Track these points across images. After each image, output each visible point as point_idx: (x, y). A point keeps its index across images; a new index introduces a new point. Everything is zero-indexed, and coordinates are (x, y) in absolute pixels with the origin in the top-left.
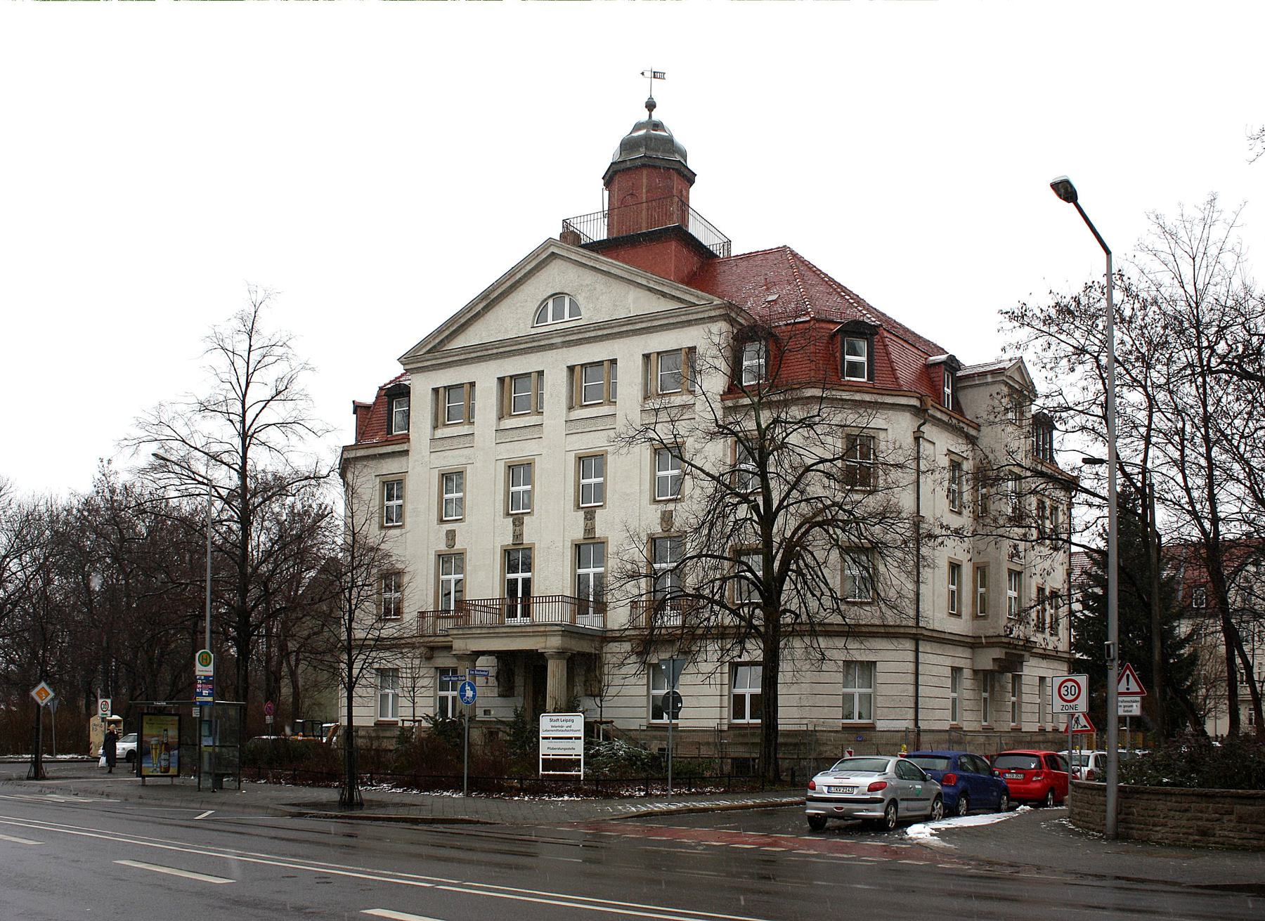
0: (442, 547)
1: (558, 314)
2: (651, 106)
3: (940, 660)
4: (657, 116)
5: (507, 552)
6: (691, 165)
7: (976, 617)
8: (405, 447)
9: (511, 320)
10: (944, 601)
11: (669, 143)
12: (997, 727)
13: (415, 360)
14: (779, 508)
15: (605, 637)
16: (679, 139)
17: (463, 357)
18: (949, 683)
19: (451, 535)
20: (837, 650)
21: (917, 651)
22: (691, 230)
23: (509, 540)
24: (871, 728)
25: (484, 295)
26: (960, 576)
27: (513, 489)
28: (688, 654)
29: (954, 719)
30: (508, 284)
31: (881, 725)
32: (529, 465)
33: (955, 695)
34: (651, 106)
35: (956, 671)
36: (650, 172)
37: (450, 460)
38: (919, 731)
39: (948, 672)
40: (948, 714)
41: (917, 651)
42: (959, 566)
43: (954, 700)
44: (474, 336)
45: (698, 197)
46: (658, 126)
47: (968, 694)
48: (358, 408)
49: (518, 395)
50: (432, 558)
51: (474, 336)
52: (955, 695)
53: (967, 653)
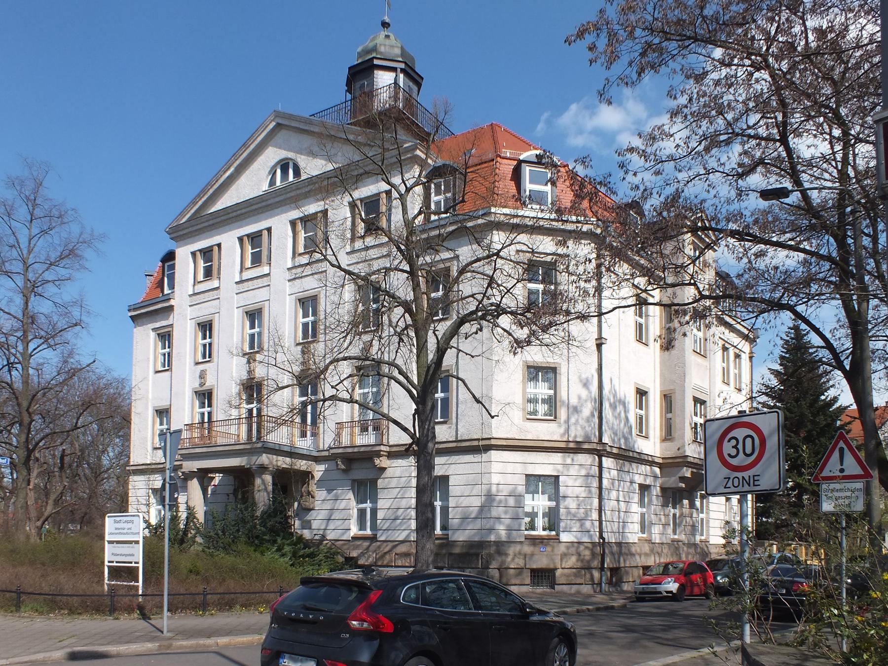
17: (211, 222)
19: (202, 375)
37: (203, 312)
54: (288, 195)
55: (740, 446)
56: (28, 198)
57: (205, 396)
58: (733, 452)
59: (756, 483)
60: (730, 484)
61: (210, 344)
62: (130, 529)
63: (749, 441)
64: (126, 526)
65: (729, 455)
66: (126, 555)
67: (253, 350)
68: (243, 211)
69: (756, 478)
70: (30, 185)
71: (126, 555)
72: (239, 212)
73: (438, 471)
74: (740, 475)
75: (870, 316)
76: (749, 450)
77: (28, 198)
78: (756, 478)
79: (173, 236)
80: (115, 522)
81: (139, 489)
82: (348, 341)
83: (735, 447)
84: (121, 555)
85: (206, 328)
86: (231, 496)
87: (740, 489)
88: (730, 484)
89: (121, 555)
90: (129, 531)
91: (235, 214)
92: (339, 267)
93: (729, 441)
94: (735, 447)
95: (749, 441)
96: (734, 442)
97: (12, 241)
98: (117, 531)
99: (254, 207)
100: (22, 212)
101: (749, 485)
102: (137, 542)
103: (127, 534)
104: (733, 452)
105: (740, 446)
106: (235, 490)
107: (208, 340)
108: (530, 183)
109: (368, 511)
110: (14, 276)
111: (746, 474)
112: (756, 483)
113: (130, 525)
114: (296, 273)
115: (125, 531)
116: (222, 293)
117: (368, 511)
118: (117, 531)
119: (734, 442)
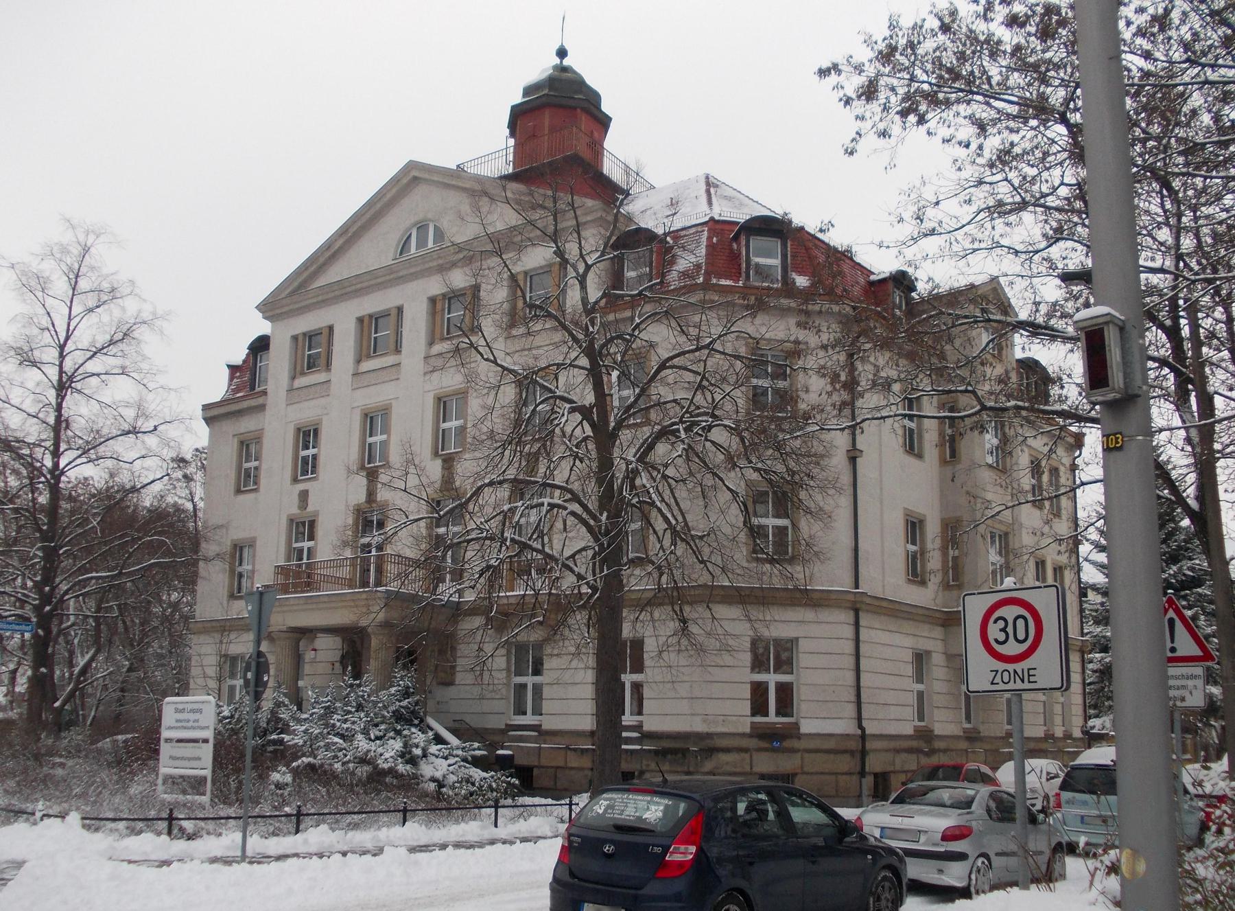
0: (294, 510)
1: (422, 242)
2: (562, 53)
3: (898, 639)
4: (566, 62)
5: (359, 511)
6: (606, 107)
7: (946, 586)
8: (260, 401)
9: (375, 253)
10: (898, 564)
11: (579, 84)
12: (986, 730)
13: (271, 307)
14: (620, 425)
15: (457, 611)
16: (591, 81)
17: (320, 298)
18: (909, 670)
19: (304, 495)
20: (734, 623)
21: (857, 625)
22: (605, 171)
23: (361, 497)
24: (793, 732)
25: (343, 230)
26: (923, 534)
27: (370, 440)
28: (555, 629)
29: (921, 718)
30: (368, 216)
31: (807, 727)
32: (385, 411)
33: (920, 687)
34: (562, 53)
35: (920, 659)
36: (559, 121)
37: (305, 412)
38: (863, 737)
39: (908, 656)
40: (910, 712)
41: (857, 625)
42: (921, 522)
43: (920, 695)
44: (338, 272)
45: (613, 143)
46: (565, 69)
47: (939, 686)
48: (233, 369)
49: (377, 334)
50: (284, 522)
51: (338, 272)
52: (920, 687)
53: (938, 632)
54: (427, 266)
55: (1010, 629)
56: (71, 269)
57: (304, 527)
58: (1002, 637)
59: (1032, 679)
60: (998, 680)
61: (315, 457)
62: (197, 721)
63: (1020, 623)
64: (192, 716)
65: (996, 641)
66: (189, 759)
67: (370, 466)
68: (366, 284)
69: (1032, 672)
70: (76, 250)
71: (189, 759)
72: (359, 286)
73: (627, 632)
74: (1011, 667)
75: (1172, 379)
76: (1021, 636)
77: (71, 269)
78: (1032, 672)
79: (270, 314)
80: (177, 710)
81: (204, 654)
82: (505, 461)
83: (1004, 630)
84: (182, 758)
85: (308, 435)
86: (337, 665)
87: (1011, 686)
88: (998, 680)
89: (182, 758)
90: (196, 724)
91: (353, 288)
92: (495, 362)
93: (995, 622)
94: (1004, 630)
95: (1020, 623)
96: (1001, 624)
97: (45, 322)
98: (179, 724)
99: (379, 280)
100: (60, 286)
101: (1023, 681)
102: (206, 741)
103: (193, 728)
104: (1002, 637)
105: (1010, 629)
106: (343, 657)
107: (311, 452)
108: (767, 715)
109: (530, 687)
110: (45, 368)
111: (1019, 667)
112: (1032, 679)
113: (197, 716)
114: (432, 366)
115: (191, 724)
116: (334, 387)
117: (530, 687)
118: (179, 724)
119: (1001, 624)
